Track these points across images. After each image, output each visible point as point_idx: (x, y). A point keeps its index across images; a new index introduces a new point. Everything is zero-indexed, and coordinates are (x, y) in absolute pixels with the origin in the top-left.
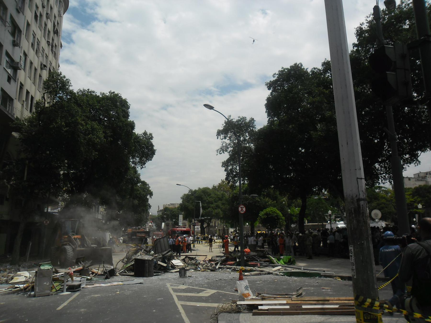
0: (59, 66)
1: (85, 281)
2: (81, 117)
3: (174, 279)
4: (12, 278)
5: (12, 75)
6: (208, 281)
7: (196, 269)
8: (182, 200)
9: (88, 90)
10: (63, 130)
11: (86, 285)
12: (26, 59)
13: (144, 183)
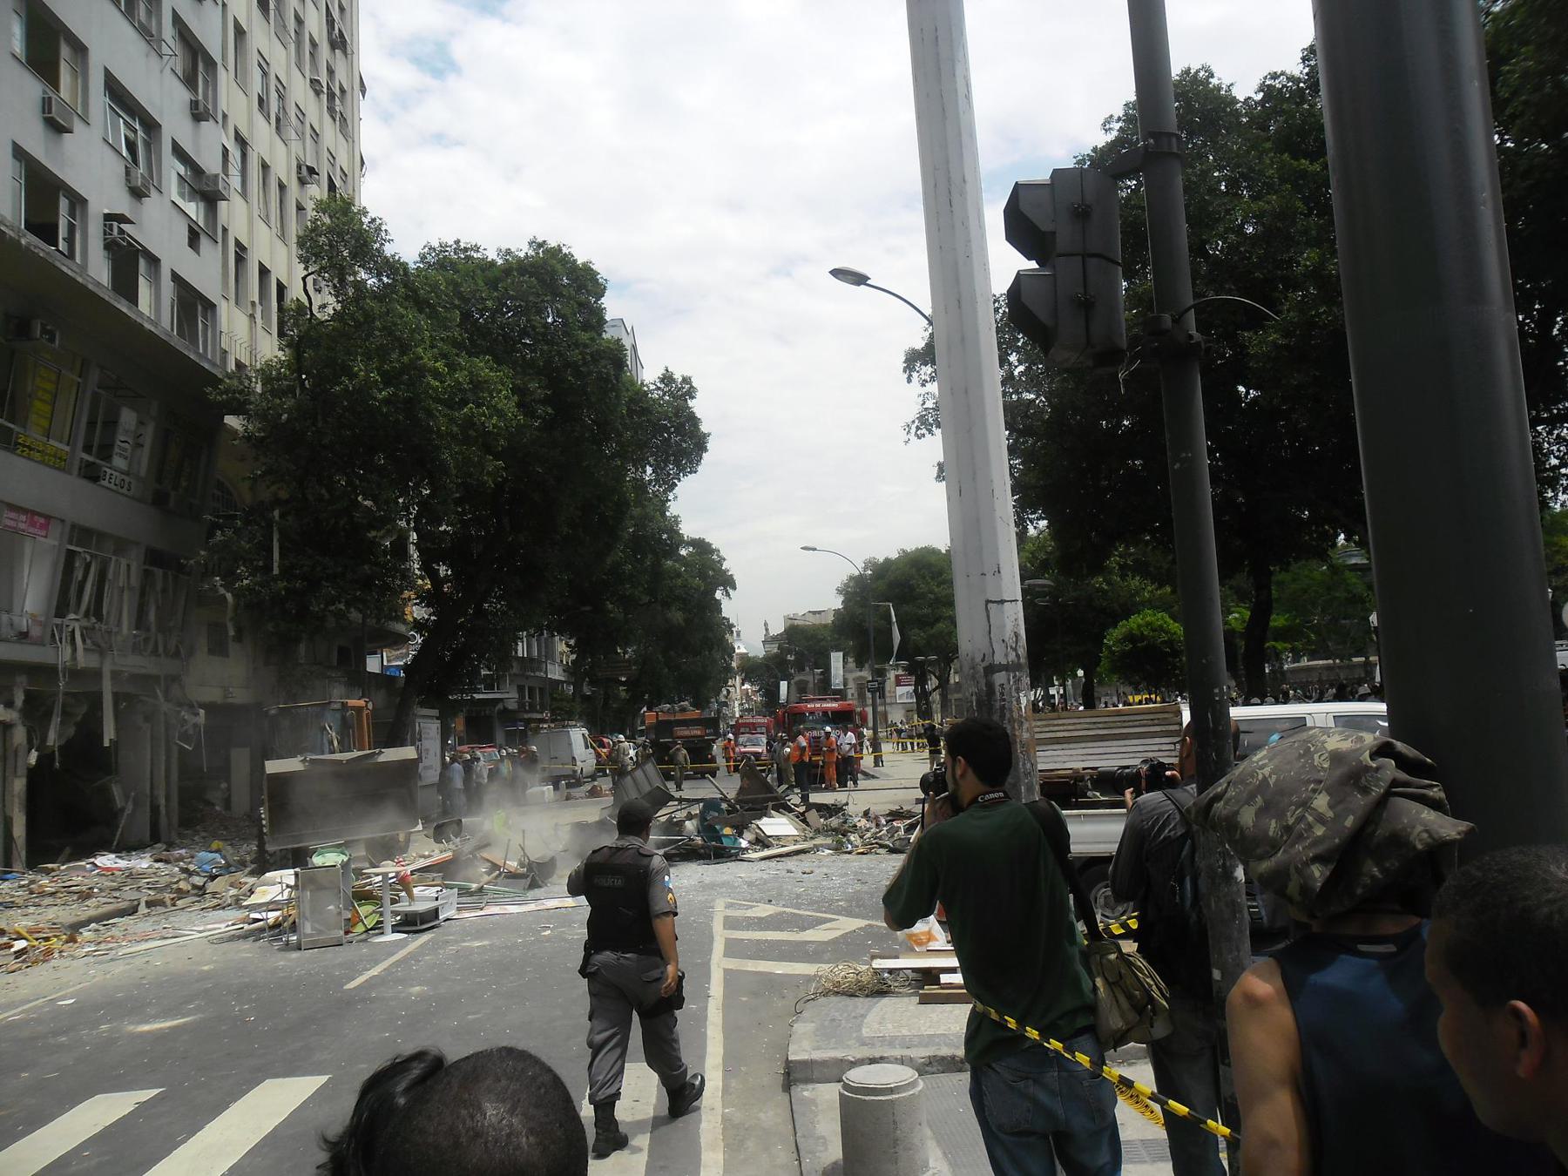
0: (363, 163)
1: (455, 899)
2: (432, 347)
3: (750, 884)
4: (251, 892)
5: (201, 223)
6: (858, 887)
7: (838, 848)
8: (841, 598)
9: (457, 242)
10: (375, 399)
11: (459, 909)
12: (244, 156)
13: (702, 547)
